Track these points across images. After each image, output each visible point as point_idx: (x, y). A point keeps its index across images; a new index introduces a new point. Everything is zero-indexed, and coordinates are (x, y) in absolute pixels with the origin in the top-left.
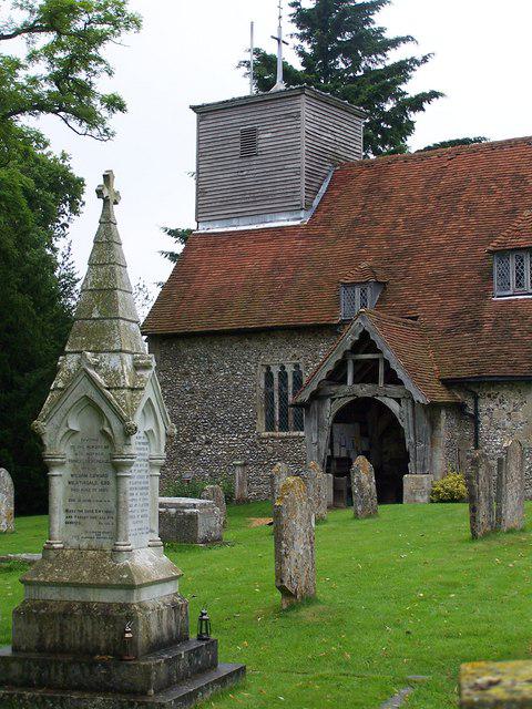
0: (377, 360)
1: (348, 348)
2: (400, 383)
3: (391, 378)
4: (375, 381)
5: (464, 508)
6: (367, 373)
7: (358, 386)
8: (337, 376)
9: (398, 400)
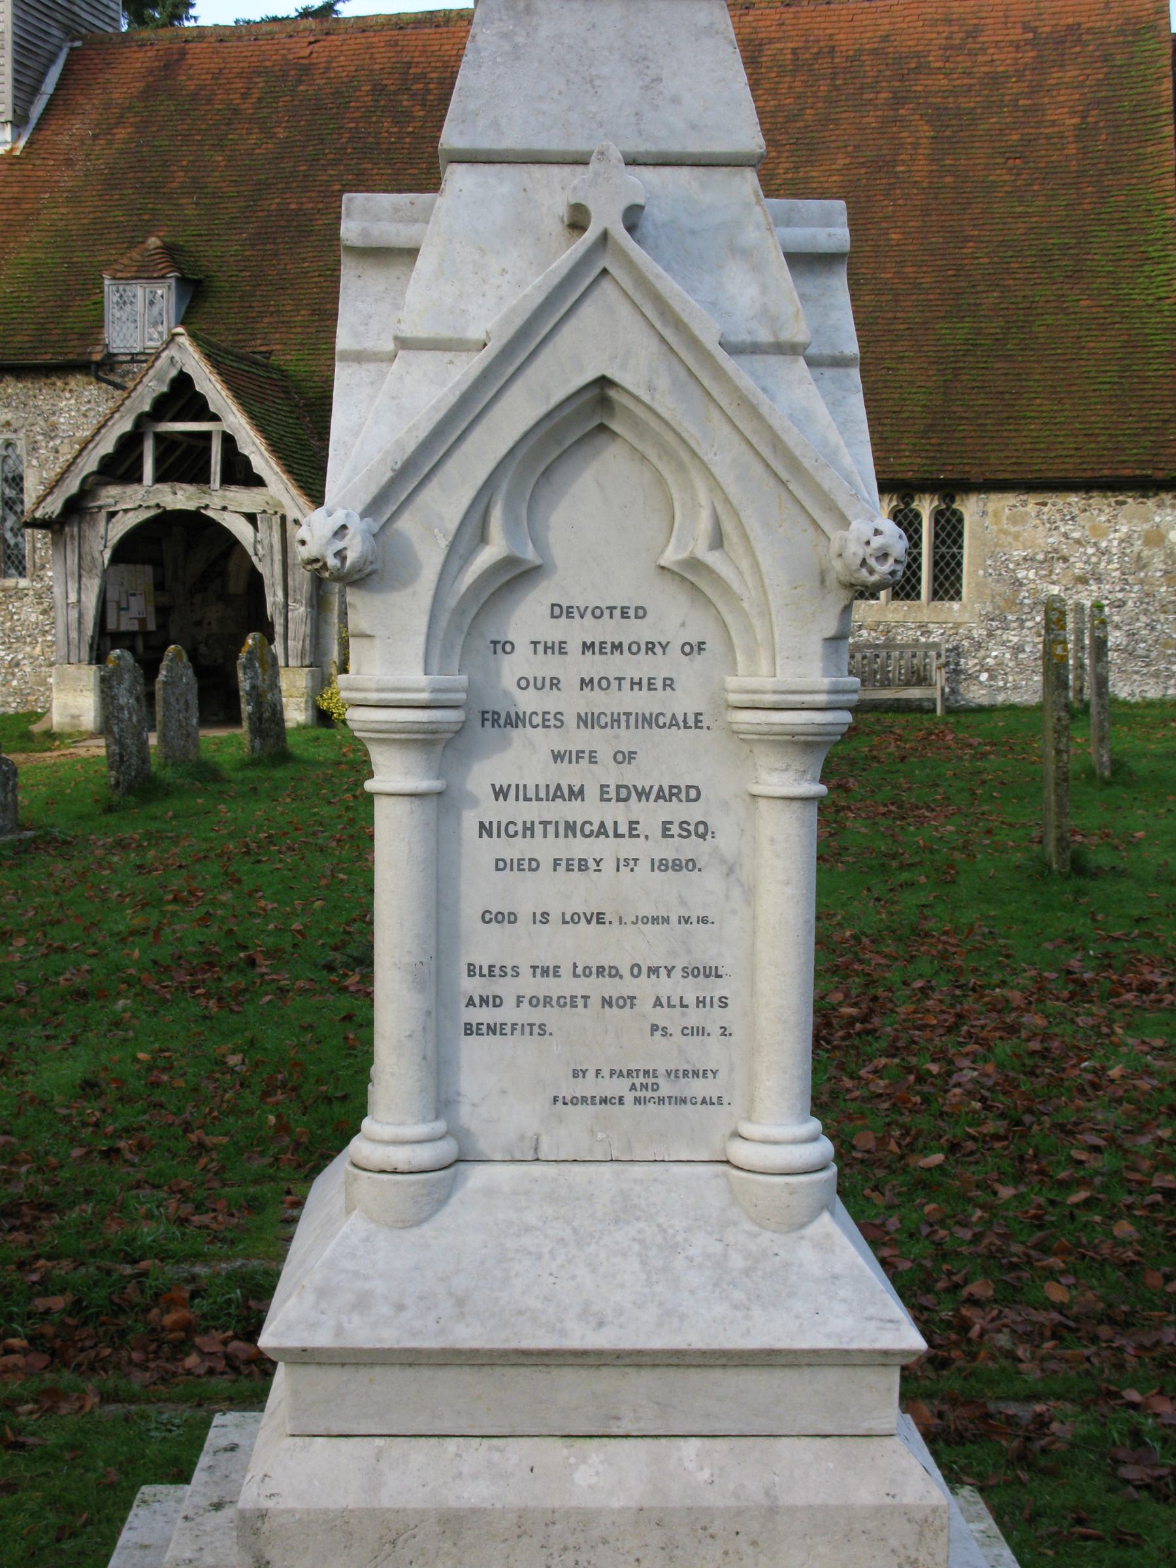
0: (207, 436)
1: (147, 408)
2: (259, 482)
3: (240, 473)
4: (200, 477)
5: (970, 508)
6: (185, 462)
7: (165, 487)
8: (120, 466)
9: (251, 518)
